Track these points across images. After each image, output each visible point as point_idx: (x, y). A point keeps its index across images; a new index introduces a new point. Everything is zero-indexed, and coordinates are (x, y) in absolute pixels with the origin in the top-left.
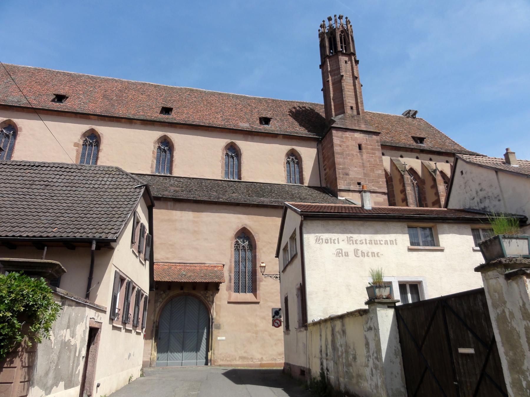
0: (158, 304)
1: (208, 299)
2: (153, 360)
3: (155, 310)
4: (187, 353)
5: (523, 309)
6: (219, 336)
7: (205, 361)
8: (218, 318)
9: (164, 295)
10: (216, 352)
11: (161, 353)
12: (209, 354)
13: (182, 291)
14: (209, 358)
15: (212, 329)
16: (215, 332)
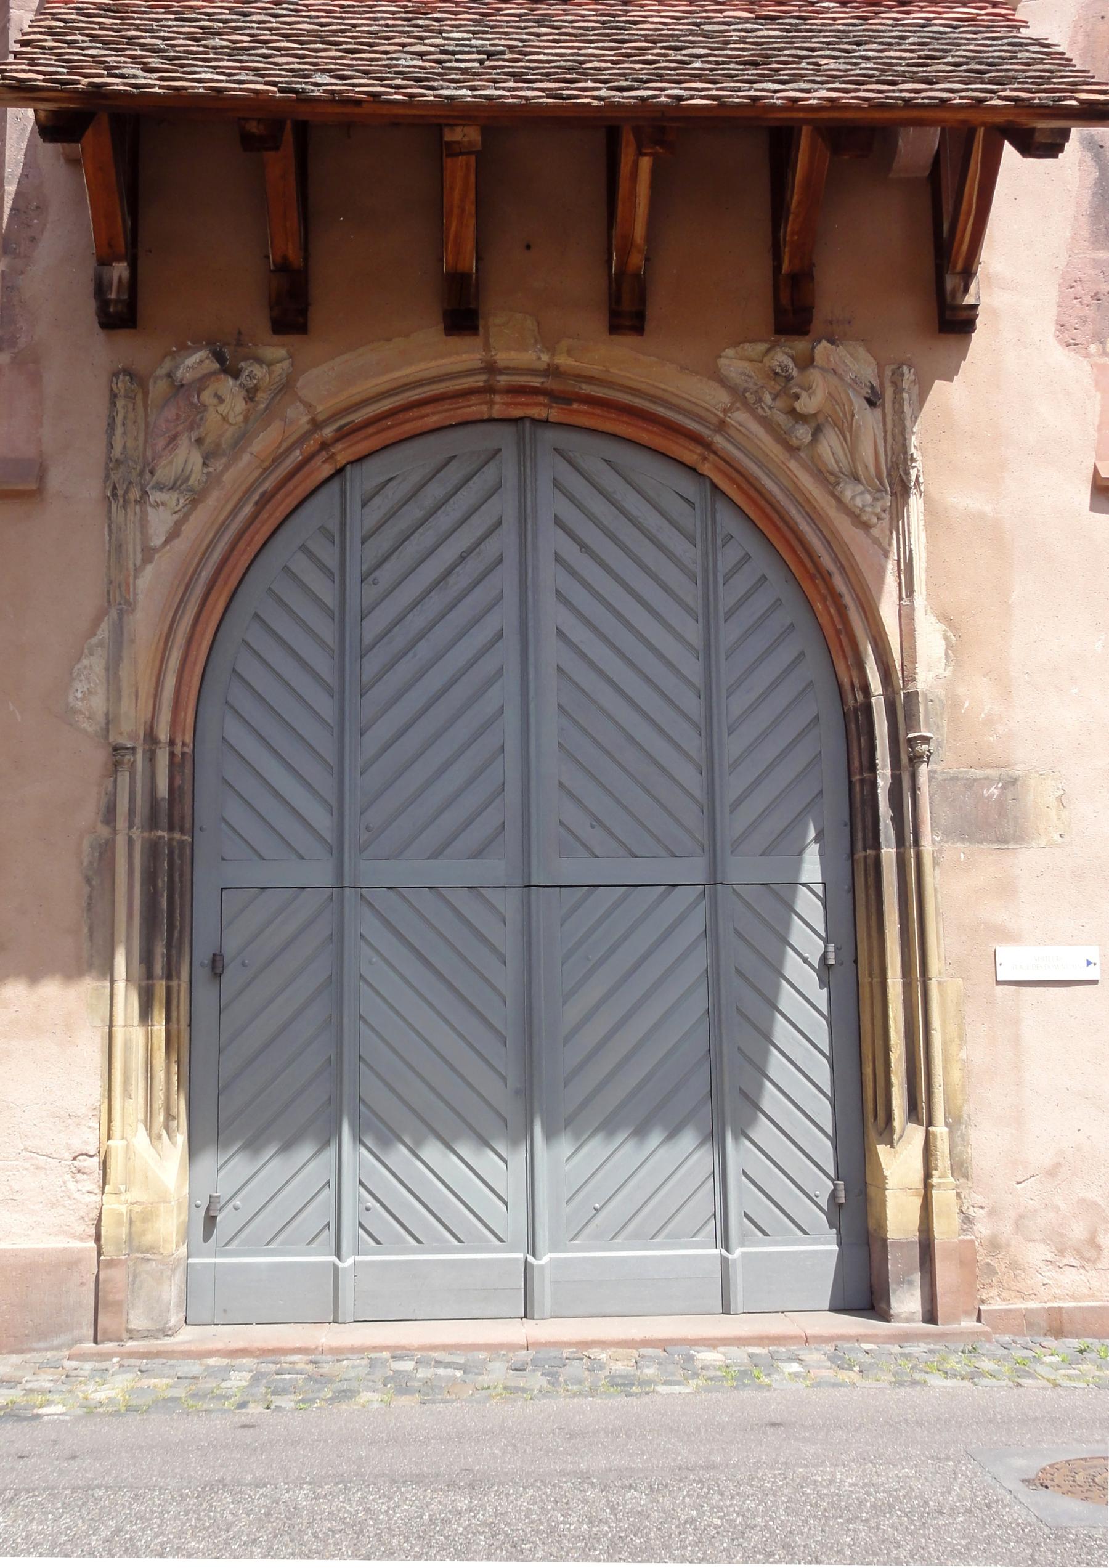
0: (160, 522)
1: (830, 448)
2: (139, 1248)
3: (117, 600)
4: (596, 1149)
5: (29, 364)
6: (1008, 936)
7: (825, 1248)
8: (979, 695)
9: (227, 402)
10: (986, 1143)
11: (253, 1145)
12: (899, 1164)
13: (462, 356)
14: (900, 1218)
15: (908, 836)
16: (955, 880)
